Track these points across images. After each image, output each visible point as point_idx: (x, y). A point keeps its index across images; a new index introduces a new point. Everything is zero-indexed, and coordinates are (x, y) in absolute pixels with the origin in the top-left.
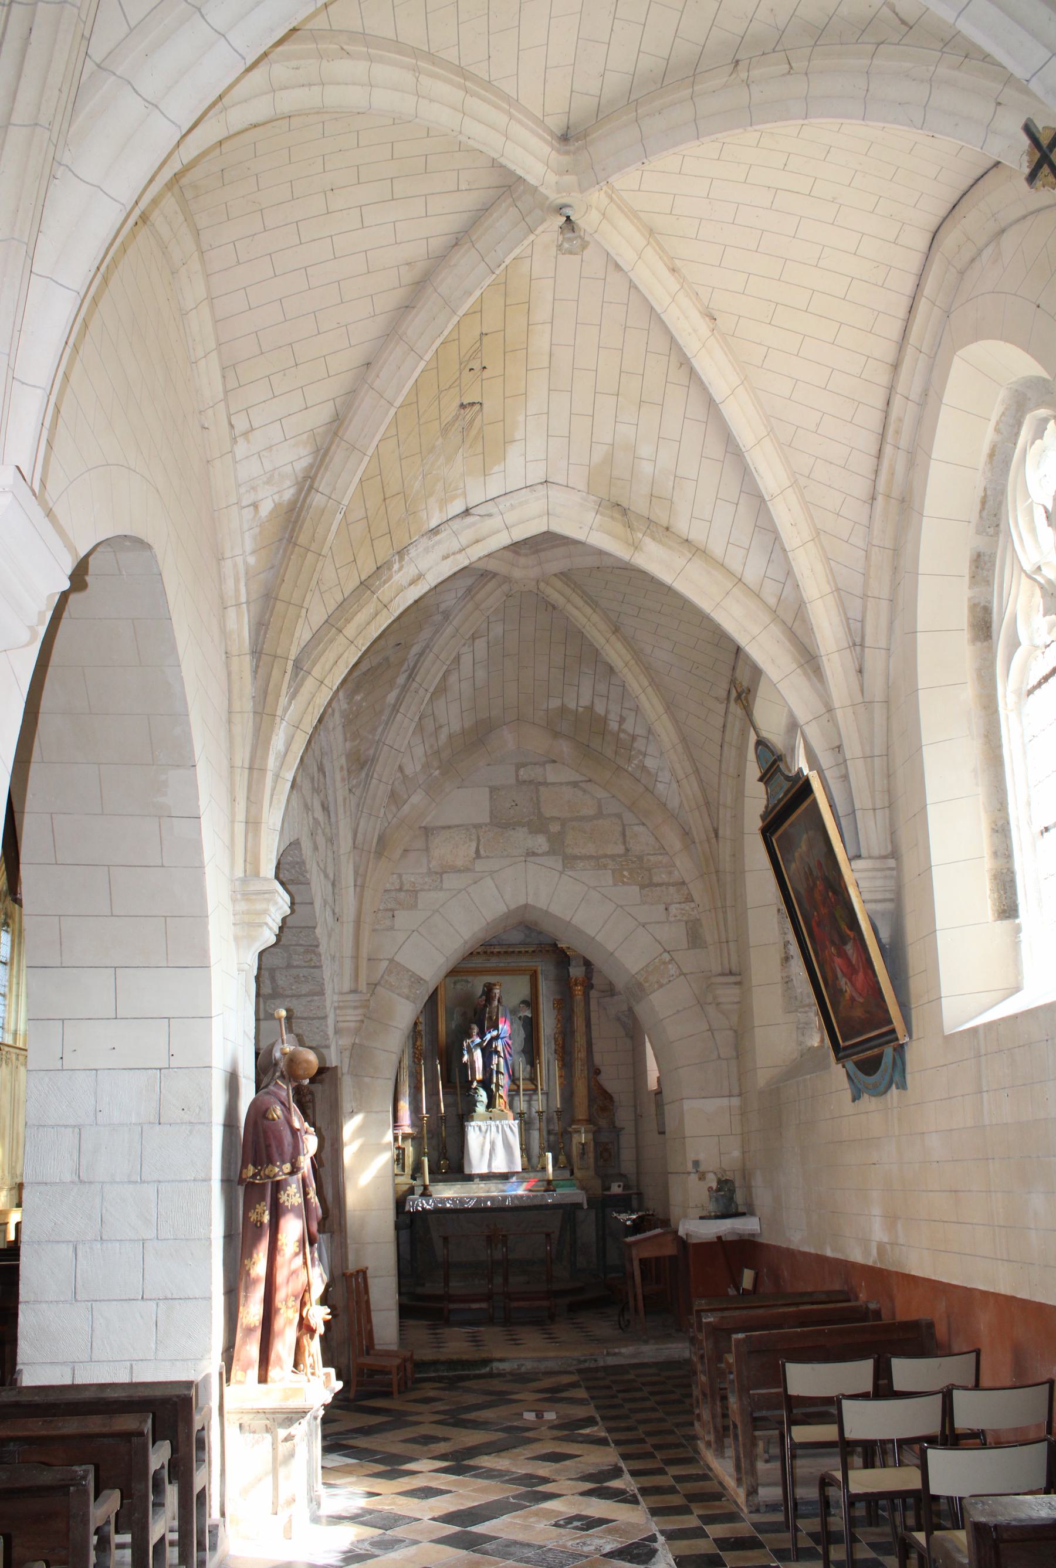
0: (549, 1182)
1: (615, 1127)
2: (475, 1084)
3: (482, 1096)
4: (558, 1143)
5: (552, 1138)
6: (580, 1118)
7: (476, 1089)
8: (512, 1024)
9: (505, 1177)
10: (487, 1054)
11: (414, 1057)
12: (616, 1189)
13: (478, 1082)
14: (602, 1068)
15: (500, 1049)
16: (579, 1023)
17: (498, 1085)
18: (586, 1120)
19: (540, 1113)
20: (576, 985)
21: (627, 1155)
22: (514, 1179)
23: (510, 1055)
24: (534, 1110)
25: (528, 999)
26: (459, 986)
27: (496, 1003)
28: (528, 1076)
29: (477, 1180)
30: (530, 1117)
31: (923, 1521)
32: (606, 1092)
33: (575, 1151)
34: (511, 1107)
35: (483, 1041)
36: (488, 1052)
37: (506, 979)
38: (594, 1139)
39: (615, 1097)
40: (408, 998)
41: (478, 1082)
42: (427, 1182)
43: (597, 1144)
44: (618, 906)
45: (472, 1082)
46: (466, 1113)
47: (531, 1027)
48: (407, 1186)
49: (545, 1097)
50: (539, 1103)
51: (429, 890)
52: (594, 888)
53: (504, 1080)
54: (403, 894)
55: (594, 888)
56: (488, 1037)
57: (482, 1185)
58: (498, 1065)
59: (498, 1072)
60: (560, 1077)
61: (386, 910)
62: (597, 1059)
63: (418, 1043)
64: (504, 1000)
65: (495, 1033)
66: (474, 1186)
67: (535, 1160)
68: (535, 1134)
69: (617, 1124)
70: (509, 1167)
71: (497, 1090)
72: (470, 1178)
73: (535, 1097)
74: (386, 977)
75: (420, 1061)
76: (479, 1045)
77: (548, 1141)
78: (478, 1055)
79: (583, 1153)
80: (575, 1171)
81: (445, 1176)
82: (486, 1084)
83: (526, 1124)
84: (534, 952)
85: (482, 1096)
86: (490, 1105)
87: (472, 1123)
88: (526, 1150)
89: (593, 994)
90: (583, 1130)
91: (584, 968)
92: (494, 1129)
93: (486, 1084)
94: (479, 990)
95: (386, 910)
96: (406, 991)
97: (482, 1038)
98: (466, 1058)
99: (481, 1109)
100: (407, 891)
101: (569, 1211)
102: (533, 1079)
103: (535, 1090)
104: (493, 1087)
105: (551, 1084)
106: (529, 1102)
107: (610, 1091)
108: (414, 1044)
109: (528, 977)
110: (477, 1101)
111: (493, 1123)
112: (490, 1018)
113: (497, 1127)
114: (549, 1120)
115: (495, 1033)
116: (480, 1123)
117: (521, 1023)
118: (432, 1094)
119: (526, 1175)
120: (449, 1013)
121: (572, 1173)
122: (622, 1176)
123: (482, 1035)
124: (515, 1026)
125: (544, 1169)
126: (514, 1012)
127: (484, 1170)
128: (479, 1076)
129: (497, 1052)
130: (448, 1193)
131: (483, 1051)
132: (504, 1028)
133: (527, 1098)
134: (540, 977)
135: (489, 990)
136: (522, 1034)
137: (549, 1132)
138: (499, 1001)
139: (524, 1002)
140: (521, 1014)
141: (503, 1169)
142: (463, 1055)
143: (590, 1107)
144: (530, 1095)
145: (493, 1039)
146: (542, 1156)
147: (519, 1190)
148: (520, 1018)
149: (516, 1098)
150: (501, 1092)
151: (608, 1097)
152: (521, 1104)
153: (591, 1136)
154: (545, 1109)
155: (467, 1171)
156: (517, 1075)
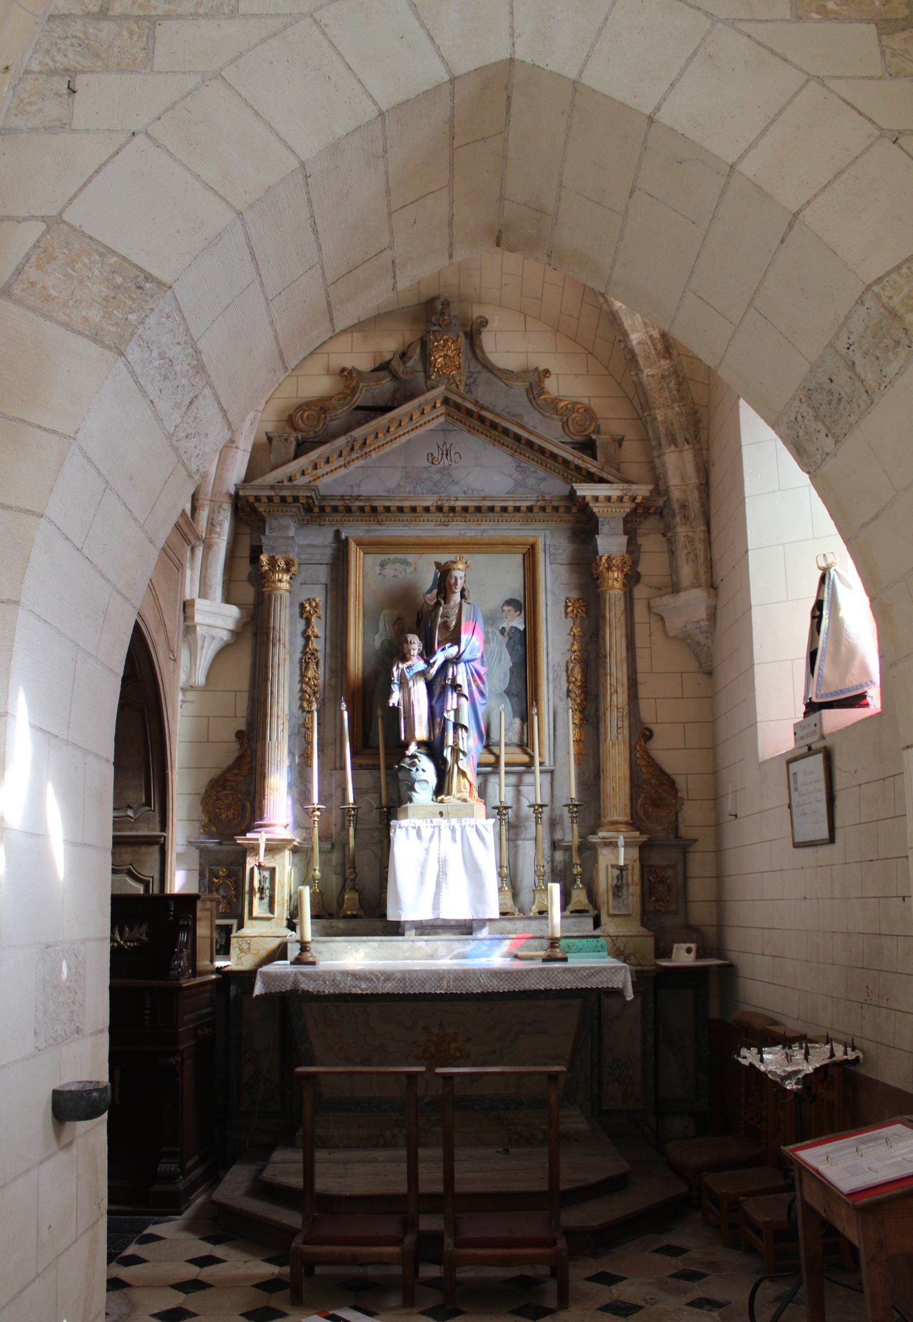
0: (554, 942)
1: (677, 837)
2: (413, 749)
3: (426, 770)
4: (572, 869)
5: (559, 856)
6: (615, 818)
7: (414, 756)
8: (487, 641)
9: (466, 928)
10: (437, 692)
11: (302, 699)
12: (683, 956)
13: (420, 744)
14: (656, 729)
15: (461, 679)
16: (614, 639)
17: (456, 751)
18: (627, 823)
19: (538, 808)
20: (609, 568)
21: (699, 890)
22: (484, 933)
23: (482, 694)
24: (525, 803)
25: (519, 597)
26: (389, 571)
27: (457, 597)
28: (515, 739)
29: (410, 934)
30: (517, 816)
31: (369, 762)
32: (661, 771)
33: (604, 880)
34: (482, 793)
35: (430, 665)
36: (439, 687)
37: (478, 560)
38: (642, 858)
39: (681, 782)
40: (96, 338)
41: (420, 744)
42: (308, 937)
43: (645, 868)
44: (810, 78)
45: (406, 746)
46: (392, 801)
47: (525, 648)
48: (277, 942)
49: (548, 777)
50: (536, 789)
51: (196, 16)
52: (731, 23)
53: (470, 742)
54: (108, 27)
55: (731, 23)
56: (439, 658)
57: (423, 944)
58: (457, 712)
59: (457, 726)
60: (577, 742)
61: (52, 73)
62: (647, 713)
63: (310, 674)
64: (472, 596)
65: (452, 651)
66: (405, 945)
67: (526, 896)
68: (527, 849)
69: (683, 832)
70: (476, 911)
71: (456, 760)
72: (396, 929)
73: (527, 779)
74: (32, 274)
75: (310, 702)
76: (422, 673)
77: (552, 861)
78: (419, 692)
79: (617, 890)
80: (604, 918)
81: (354, 923)
82: (433, 749)
83: (511, 827)
84: (530, 509)
85: (426, 770)
86: (441, 789)
87: (403, 822)
88: (510, 879)
89: (640, 592)
90: (621, 841)
91: (624, 539)
92: (446, 834)
93: (433, 749)
94: (427, 577)
95: (52, 73)
96: (95, 315)
97: (427, 662)
98: (396, 698)
99: (423, 794)
100: (125, 17)
101: (591, 1001)
102: (525, 745)
103: (529, 765)
104: (447, 753)
105: (560, 754)
106: (517, 786)
107: (668, 769)
108: (303, 675)
109: (519, 557)
110: (413, 781)
111: (443, 822)
112: (445, 625)
113: (453, 830)
114: (553, 824)
115: (452, 651)
116: (419, 823)
117: (504, 640)
118: (332, 767)
119: (507, 925)
120: (371, 619)
121: (597, 924)
122: (691, 932)
123: (428, 653)
124: (493, 645)
125: (543, 913)
126: (490, 620)
127: (424, 913)
128: (421, 732)
129: (456, 687)
130: (353, 958)
131: (430, 685)
132: (472, 642)
133: (513, 779)
134: (540, 555)
135: (444, 583)
136: (507, 662)
137: (554, 846)
138: (463, 596)
139: (510, 602)
140: (506, 624)
141: (464, 913)
142: (390, 692)
143: (633, 799)
144: (520, 774)
145: (446, 663)
146: (540, 890)
147: (491, 957)
148: (503, 631)
149: (493, 780)
150: (463, 764)
151: (667, 782)
152: (502, 789)
153: (635, 853)
154: (547, 801)
155: (391, 917)
156: (494, 736)
